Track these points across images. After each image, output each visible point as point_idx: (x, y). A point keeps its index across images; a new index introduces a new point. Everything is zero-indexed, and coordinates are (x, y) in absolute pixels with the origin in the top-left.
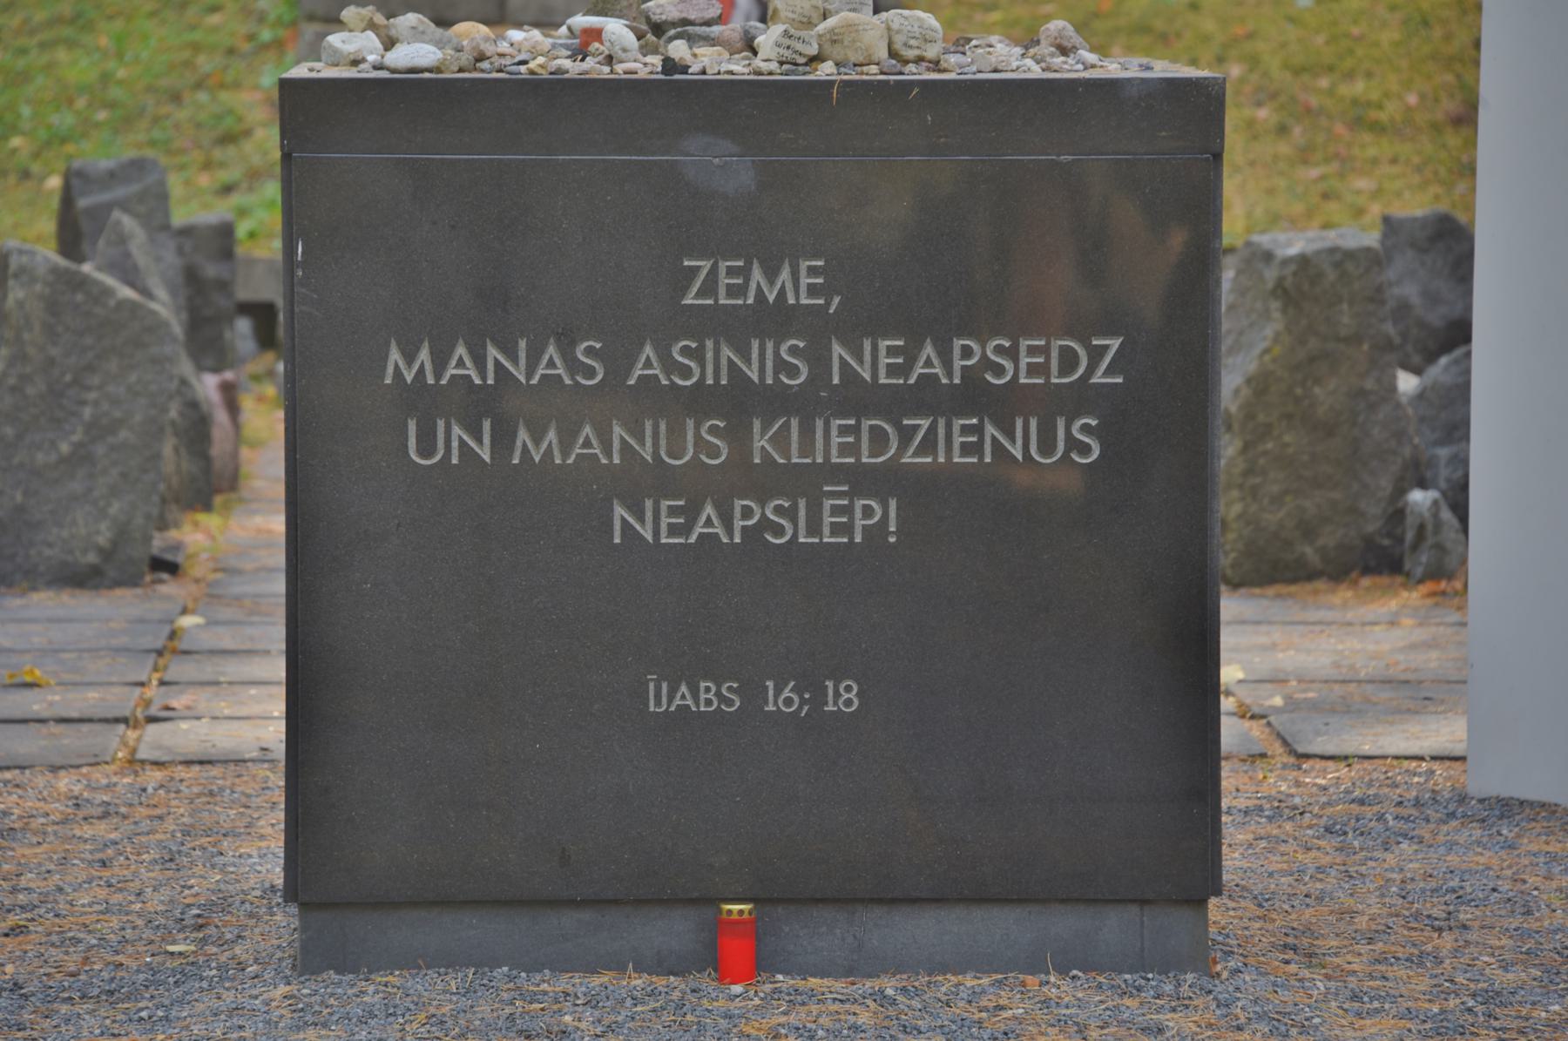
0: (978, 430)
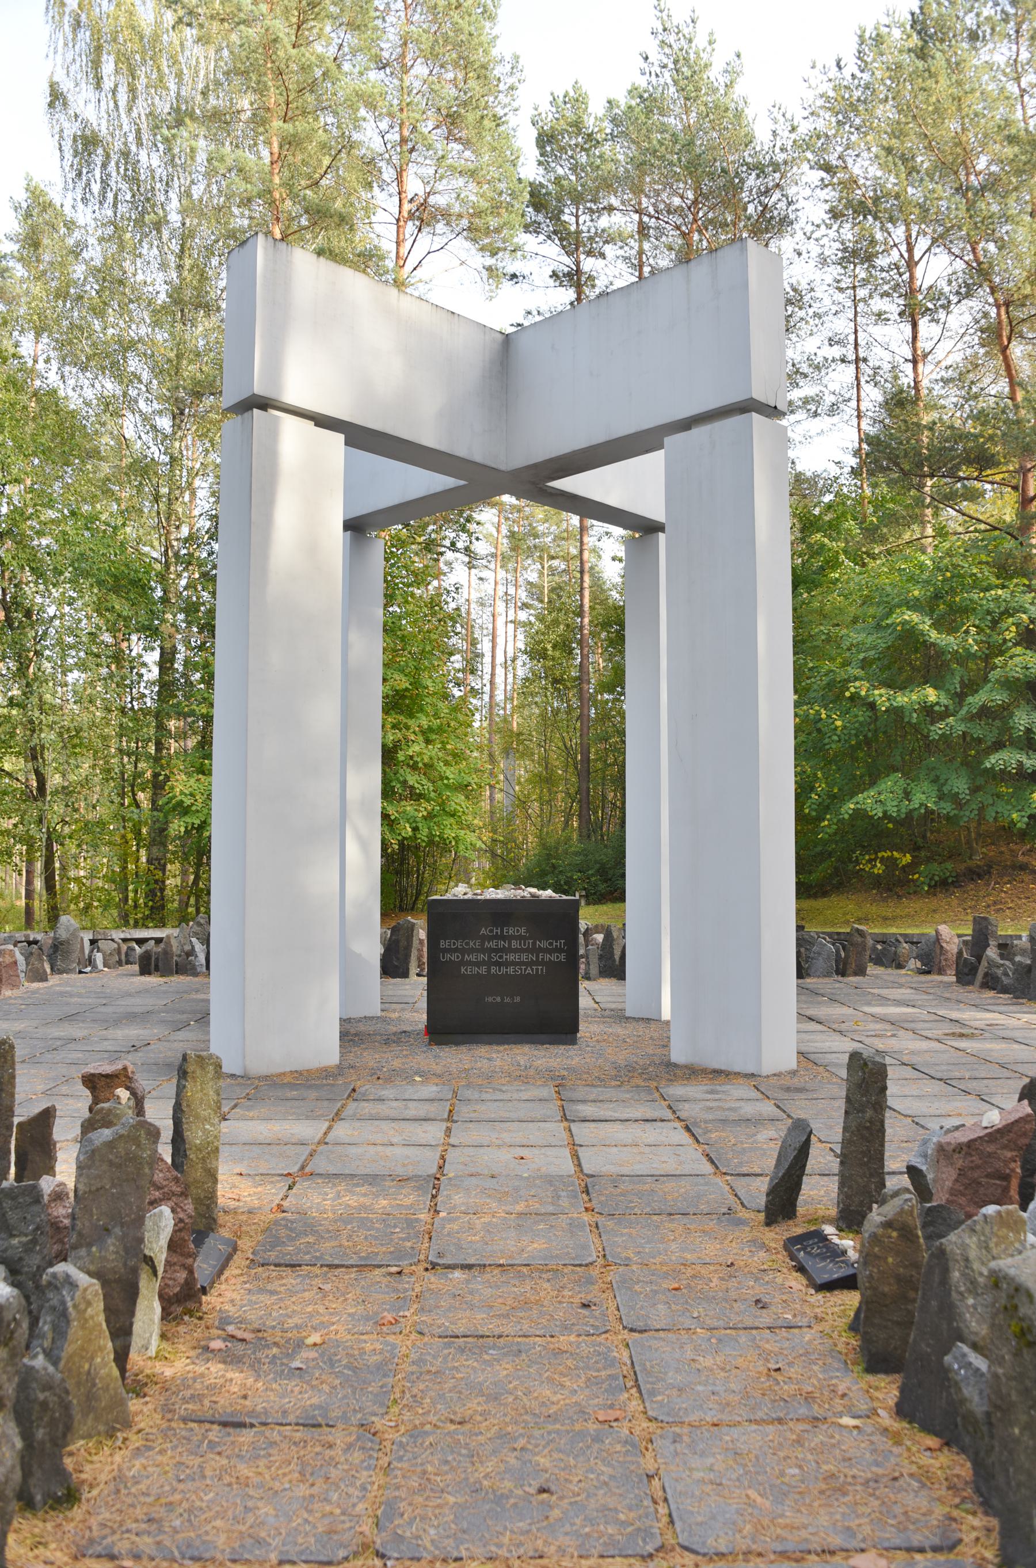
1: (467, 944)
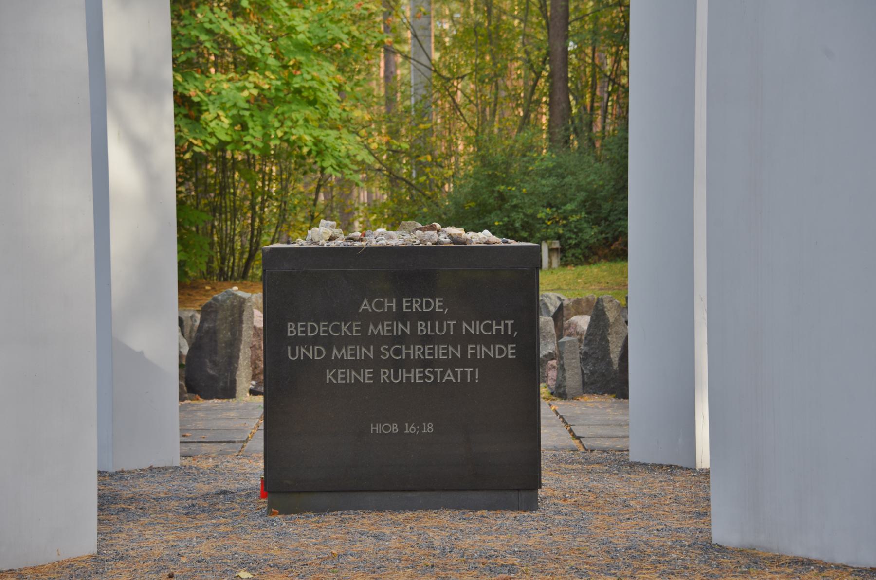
0: (447, 349)
1: (337, 329)
